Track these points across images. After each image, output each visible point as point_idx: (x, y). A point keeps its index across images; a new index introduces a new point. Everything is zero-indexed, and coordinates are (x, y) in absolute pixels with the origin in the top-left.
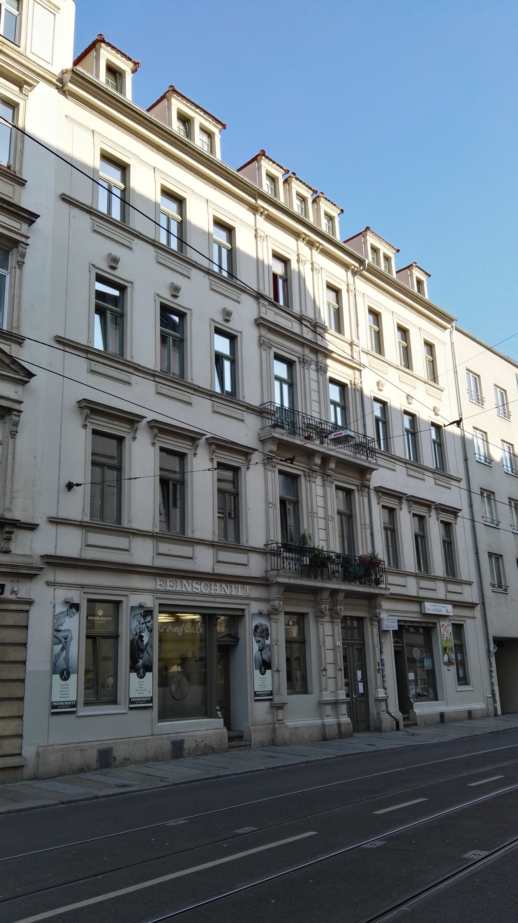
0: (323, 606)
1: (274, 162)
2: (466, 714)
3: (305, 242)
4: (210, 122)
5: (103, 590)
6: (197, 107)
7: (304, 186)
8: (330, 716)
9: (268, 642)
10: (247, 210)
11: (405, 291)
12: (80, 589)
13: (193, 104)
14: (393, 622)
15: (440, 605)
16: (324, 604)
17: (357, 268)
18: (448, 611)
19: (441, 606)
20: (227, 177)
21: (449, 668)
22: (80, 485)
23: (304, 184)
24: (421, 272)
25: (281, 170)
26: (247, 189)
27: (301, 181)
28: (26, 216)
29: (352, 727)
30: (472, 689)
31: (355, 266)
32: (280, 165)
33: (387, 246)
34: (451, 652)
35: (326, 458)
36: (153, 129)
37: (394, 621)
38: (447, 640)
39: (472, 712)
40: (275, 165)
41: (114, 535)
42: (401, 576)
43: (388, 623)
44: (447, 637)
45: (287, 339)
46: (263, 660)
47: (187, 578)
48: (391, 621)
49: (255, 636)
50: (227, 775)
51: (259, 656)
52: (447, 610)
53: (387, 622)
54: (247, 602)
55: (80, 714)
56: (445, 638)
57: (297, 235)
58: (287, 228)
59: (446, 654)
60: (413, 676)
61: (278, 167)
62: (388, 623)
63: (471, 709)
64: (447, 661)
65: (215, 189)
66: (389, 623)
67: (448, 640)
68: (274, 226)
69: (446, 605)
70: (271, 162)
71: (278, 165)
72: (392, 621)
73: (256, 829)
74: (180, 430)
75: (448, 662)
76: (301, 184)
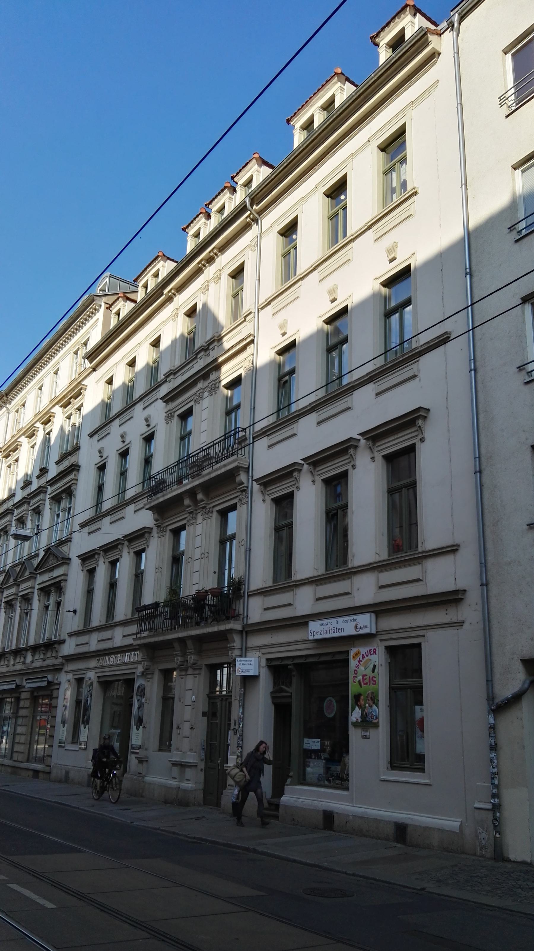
0: (175, 658)
1: (192, 222)
2: (390, 831)
3: (207, 265)
4: (156, 265)
5: (416, 632)
6: (146, 269)
7: (219, 197)
8: (189, 780)
9: (144, 700)
10: (170, 304)
11: (315, 141)
12: (258, 650)
13: (144, 271)
14: (248, 664)
15: (340, 620)
16: (189, 655)
17: (250, 214)
18: (359, 626)
19: (344, 622)
20: (146, 306)
21: (367, 734)
22: (67, 611)
23: (217, 196)
24: (392, 24)
25: (200, 217)
26: (157, 296)
27: (214, 199)
28: (62, 475)
29: (201, 796)
30: (427, 781)
31: (249, 216)
32: (195, 216)
33: (321, 93)
34: (371, 702)
35: (192, 493)
36: (116, 336)
37: (249, 663)
38: (364, 679)
39: (409, 829)
40: (195, 222)
41: (81, 636)
42: (325, 584)
43: (240, 666)
44: (364, 676)
45: (180, 395)
46: (139, 717)
47: (109, 654)
48: (245, 663)
49: (137, 696)
50: (35, 798)
51: (137, 713)
52: (357, 625)
53: (240, 664)
54: (135, 666)
55: (66, 748)
56: (361, 678)
57: (198, 271)
58: (190, 278)
59: (357, 708)
60: (319, 744)
61: (197, 219)
62: (240, 666)
63: (408, 822)
64: (360, 720)
65: (152, 320)
66: (242, 666)
67: (367, 681)
68: (187, 288)
69: (355, 617)
70: (192, 225)
71: (195, 219)
72: (247, 663)
73: (266, 894)
74: (114, 543)
75: (362, 721)
76: (216, 200)
